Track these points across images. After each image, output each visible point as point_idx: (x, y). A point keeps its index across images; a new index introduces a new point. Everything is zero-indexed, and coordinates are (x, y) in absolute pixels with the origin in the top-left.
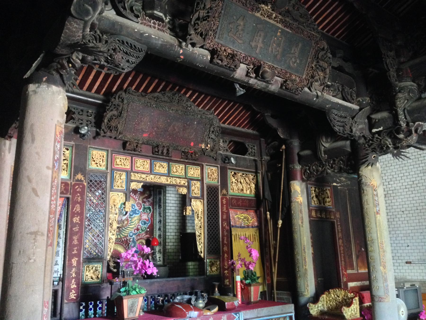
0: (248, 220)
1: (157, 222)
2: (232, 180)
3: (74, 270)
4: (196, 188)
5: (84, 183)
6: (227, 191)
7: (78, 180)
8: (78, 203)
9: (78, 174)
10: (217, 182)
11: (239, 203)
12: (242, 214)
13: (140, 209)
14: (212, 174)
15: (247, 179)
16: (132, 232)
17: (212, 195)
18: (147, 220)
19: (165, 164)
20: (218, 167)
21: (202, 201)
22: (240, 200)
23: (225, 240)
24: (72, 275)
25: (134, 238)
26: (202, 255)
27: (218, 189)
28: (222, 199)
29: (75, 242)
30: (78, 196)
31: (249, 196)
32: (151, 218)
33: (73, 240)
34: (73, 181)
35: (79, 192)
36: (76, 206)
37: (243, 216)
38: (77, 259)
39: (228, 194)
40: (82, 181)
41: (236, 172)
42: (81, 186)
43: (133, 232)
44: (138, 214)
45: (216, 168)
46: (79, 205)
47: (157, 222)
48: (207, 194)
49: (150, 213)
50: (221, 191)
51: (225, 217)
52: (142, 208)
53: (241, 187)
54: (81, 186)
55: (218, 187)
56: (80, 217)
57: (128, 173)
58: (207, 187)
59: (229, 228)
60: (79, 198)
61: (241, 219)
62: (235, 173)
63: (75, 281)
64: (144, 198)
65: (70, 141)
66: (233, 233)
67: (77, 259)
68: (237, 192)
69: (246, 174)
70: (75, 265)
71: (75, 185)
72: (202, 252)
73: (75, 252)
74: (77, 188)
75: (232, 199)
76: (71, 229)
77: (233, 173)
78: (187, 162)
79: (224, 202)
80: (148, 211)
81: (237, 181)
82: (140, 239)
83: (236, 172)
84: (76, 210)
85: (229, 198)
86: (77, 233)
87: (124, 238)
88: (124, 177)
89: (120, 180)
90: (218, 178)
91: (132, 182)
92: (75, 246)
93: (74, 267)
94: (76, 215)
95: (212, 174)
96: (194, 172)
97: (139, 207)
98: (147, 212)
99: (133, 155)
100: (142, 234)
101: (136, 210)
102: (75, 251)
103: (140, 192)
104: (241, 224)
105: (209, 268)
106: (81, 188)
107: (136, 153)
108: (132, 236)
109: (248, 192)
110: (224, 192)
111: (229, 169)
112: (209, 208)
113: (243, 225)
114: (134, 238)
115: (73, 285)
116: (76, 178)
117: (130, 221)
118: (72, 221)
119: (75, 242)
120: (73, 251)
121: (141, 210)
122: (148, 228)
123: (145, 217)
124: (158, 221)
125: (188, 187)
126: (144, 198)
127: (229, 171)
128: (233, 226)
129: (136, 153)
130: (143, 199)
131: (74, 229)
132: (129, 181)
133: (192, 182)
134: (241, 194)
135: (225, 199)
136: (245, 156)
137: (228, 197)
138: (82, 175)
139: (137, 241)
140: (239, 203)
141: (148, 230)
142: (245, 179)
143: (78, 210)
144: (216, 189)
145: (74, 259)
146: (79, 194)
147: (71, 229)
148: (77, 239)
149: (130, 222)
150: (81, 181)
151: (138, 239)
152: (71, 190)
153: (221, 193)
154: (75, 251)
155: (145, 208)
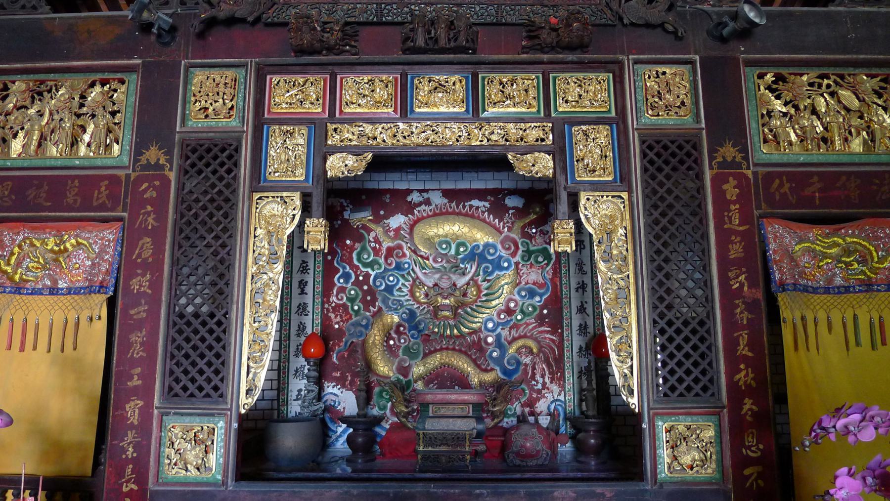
0: (863, 261)
1: (573, 291)
2: (768, 103)
3: (130, 436)
4: (593, 149)
5: (167, 173)
6: (744, 150)
7: (148, 166)
8: (147, 233)
9: (148, 149)
10: (689, 119)
11: (808, 191)
12: (827, 236)
13: (514, 255)
14: (667, 93)
15: (844, 93)
16: (491, 319)
17: (665, 169)
18: (541, 286)
19: (456, 81)
20: (691, 63)
21: (625, 195)
22: (815, 179)
23: (743, 342)
24: (125, 451)
25: (498, 337)
26: (634, 401)
27: (696, 146)
28: (717, 181)
29: (137, 352)
30: (149, 214)
31: (864, 159)
32: (552, 280)
33: (130, 345)
34: (134, 170)
35: (150, 201)
36: (141, 243)
37: (836, 245)
38: (140, 403)
39: (746, 158)
40: (162, 167)
41: (784, 71)
42: (157, 183)
43: (495, 318)
44: (507, 268)
45: (685, 69)
46: (148, 240)
47: (573, 291)
48: (645, 170)
49: (547, 265)
50: (712, 152)
51: (736, 250)
52: (520, 252)
53: (819, 129)
54: (157, 183)
55: (698, 136)
56: (152, 275)
57: (318, 129)
58: (643, 142)
59: (759, 295)
60: (150, 220)
61: (825, 256)
62: (779, 78)
63: (133, 472)
64: (530, 224)
65: (130, 57)
66: (785, 313)
67: (140, 403)
68: (796, 149)
69: (842, 77)
70: (136, 423)
71: (139, 180)
72: (631, 392)
73: (136, 382)
74: (145, 191)
75: (769, 178)
76: (125, 311)
77: (769, 78)
78: (550, 62)
79: (731, 190)
80: (540, 259)
81: (796, 107)
82: (520, 337)
83: (784, 71)
84: (139, 256)
85: (755, 174)
86: (139, 325)
87: (470, 334)
88: (300, 139)
89: (287, 154)
90: (697, 104)
91: (333, 153)
92: (134, 363)
93: (132, 427)
94: (139, 271)
95: (667, 93)
96: (583, 91)
97: (509, 249)
98: (537, 262)
99: (336, 69)
100: (528, 325)
101: (500, 257)
102: (136, 377)
103: (513, 208)
104: (830, 280)
105: (665, 454)
106: (155, 188)
107: (341, 58)
108: (493, 331)
109: (856, 145)
110: (729, 151)
111: (750, 64)
112: (656, 222)
113: (838, 281)
114: (498, 337)
115: (128, 481)
116: (143, 160)
117: (487, 289)
118: (127, 287)
119: (137, 352)
120: (131, 378)
121: (518, 258)
122: (542, 308)
123: (533, 276)
124: (574, 285)
125: (560, 151)
126: (530, 224)
127: (749, 75)
128: (783, 287)
129: (341, 58)
130: (523, 228)
131: (132, 312)
132: (320, 151)
133: (575, 129)
134: (820, 155)
135: (733, 182)
136: (832, 8)
137: (749, 173)
138: (160, 149)
139: (510, 343)
140: (808, 191)
141: (545, 312)
142: (832, 94)
143: (147, 253)
144: (688, 147)
145: (132, 404)
146: (149, 208)
147: (125, 311)
148: (142, 344)
149: (485, 292)
150: (158, 166)
151: (515, 339)
152: (126, 197)
153: (711, 158)
154: (136, 377)
155: (528, 253)
